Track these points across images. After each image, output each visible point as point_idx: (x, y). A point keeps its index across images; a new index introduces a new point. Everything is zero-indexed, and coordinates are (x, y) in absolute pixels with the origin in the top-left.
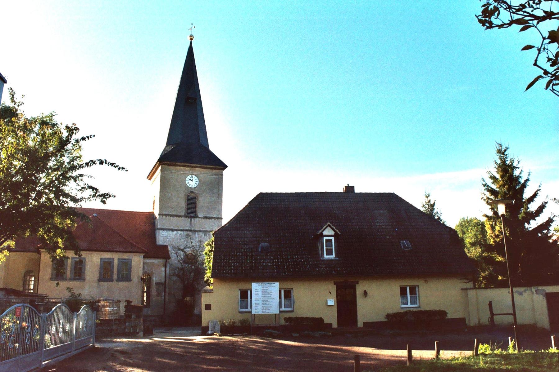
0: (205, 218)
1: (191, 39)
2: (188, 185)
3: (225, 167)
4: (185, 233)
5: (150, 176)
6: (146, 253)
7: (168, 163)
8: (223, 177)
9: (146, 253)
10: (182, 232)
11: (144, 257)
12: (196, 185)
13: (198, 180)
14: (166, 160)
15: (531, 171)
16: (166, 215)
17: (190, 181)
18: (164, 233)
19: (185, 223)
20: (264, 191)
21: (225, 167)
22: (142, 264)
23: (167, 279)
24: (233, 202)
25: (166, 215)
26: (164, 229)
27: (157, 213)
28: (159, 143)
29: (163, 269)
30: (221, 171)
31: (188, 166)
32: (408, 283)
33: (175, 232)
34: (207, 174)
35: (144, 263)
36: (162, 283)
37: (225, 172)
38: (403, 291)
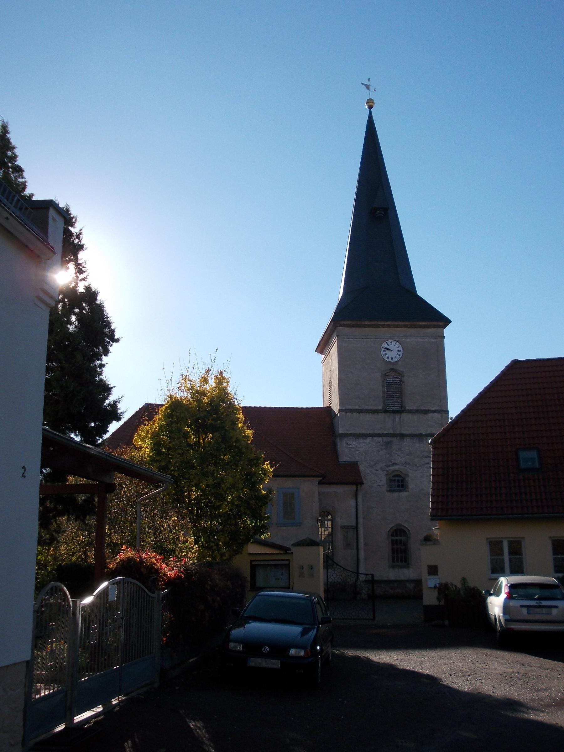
0: (417, 412)
1: (370, 107)
2: (385, 357)
3: (447, 322)
4: (386, 439)
5: (322, 347)
6: (323, 476)
7: (349, 322)
8: (446, 340)
9: (323, 476)
10: (380, 439)
11: (320, 483)
12: (398, 357)
13: (400, 349)
14: (348, 316)
15: (121, 341)
16: (352, 411)
17: (387, 352)
18: (354, 444)
19: (387, 423)
20: (522, 357)
21: (447, 322)
22: (316, 496)
23: (361, 520)
24: (464, 383)
25: (352, 411)
26: (356, 436)
27: (336, 409)
28: (331, 288)
29: (352, 502)
30: (439, 329)
31: (383, 326)
32: (505, 532)
33: (368, 440)
34: (417, 336)
35: (319, 493)
36: (352, 527)
37: (447, 331)
38: (495, 546)
